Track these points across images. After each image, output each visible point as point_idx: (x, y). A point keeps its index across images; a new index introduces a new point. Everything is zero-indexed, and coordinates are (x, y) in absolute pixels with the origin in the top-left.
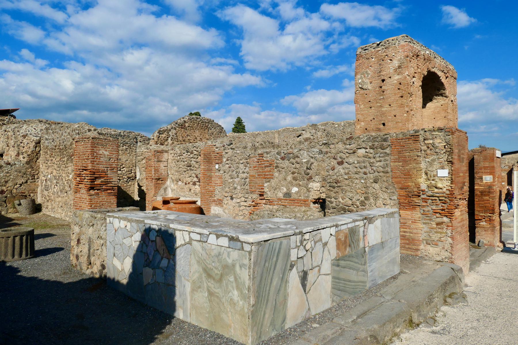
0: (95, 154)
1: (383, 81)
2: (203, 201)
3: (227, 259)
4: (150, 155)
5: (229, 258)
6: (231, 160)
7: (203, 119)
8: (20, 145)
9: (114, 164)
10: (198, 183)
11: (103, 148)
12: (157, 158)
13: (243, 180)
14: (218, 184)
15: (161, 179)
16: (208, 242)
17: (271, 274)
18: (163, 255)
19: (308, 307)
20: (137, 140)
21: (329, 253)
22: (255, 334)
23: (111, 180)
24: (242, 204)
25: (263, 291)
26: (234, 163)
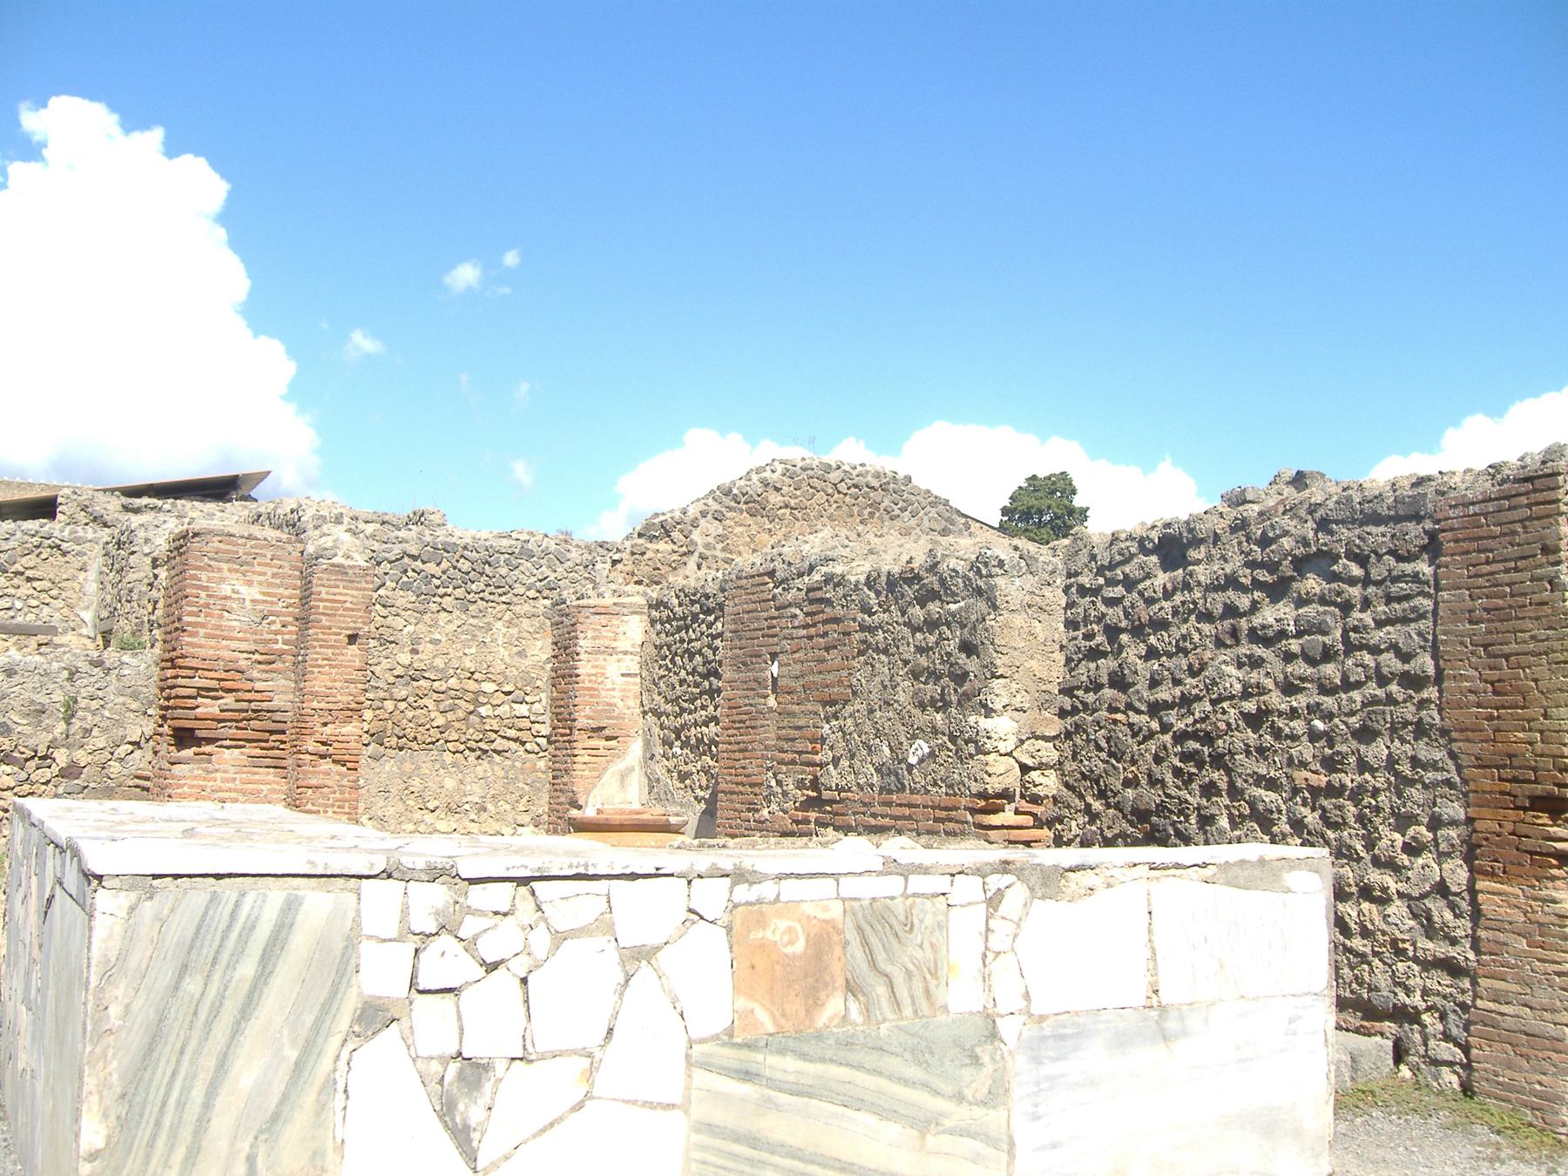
0: (203, 594)
7: (855, 473)
9: (279, 637)
11: (236, 571)
12: (594, 638)
15: (607, 732)
25: (164, 1104)
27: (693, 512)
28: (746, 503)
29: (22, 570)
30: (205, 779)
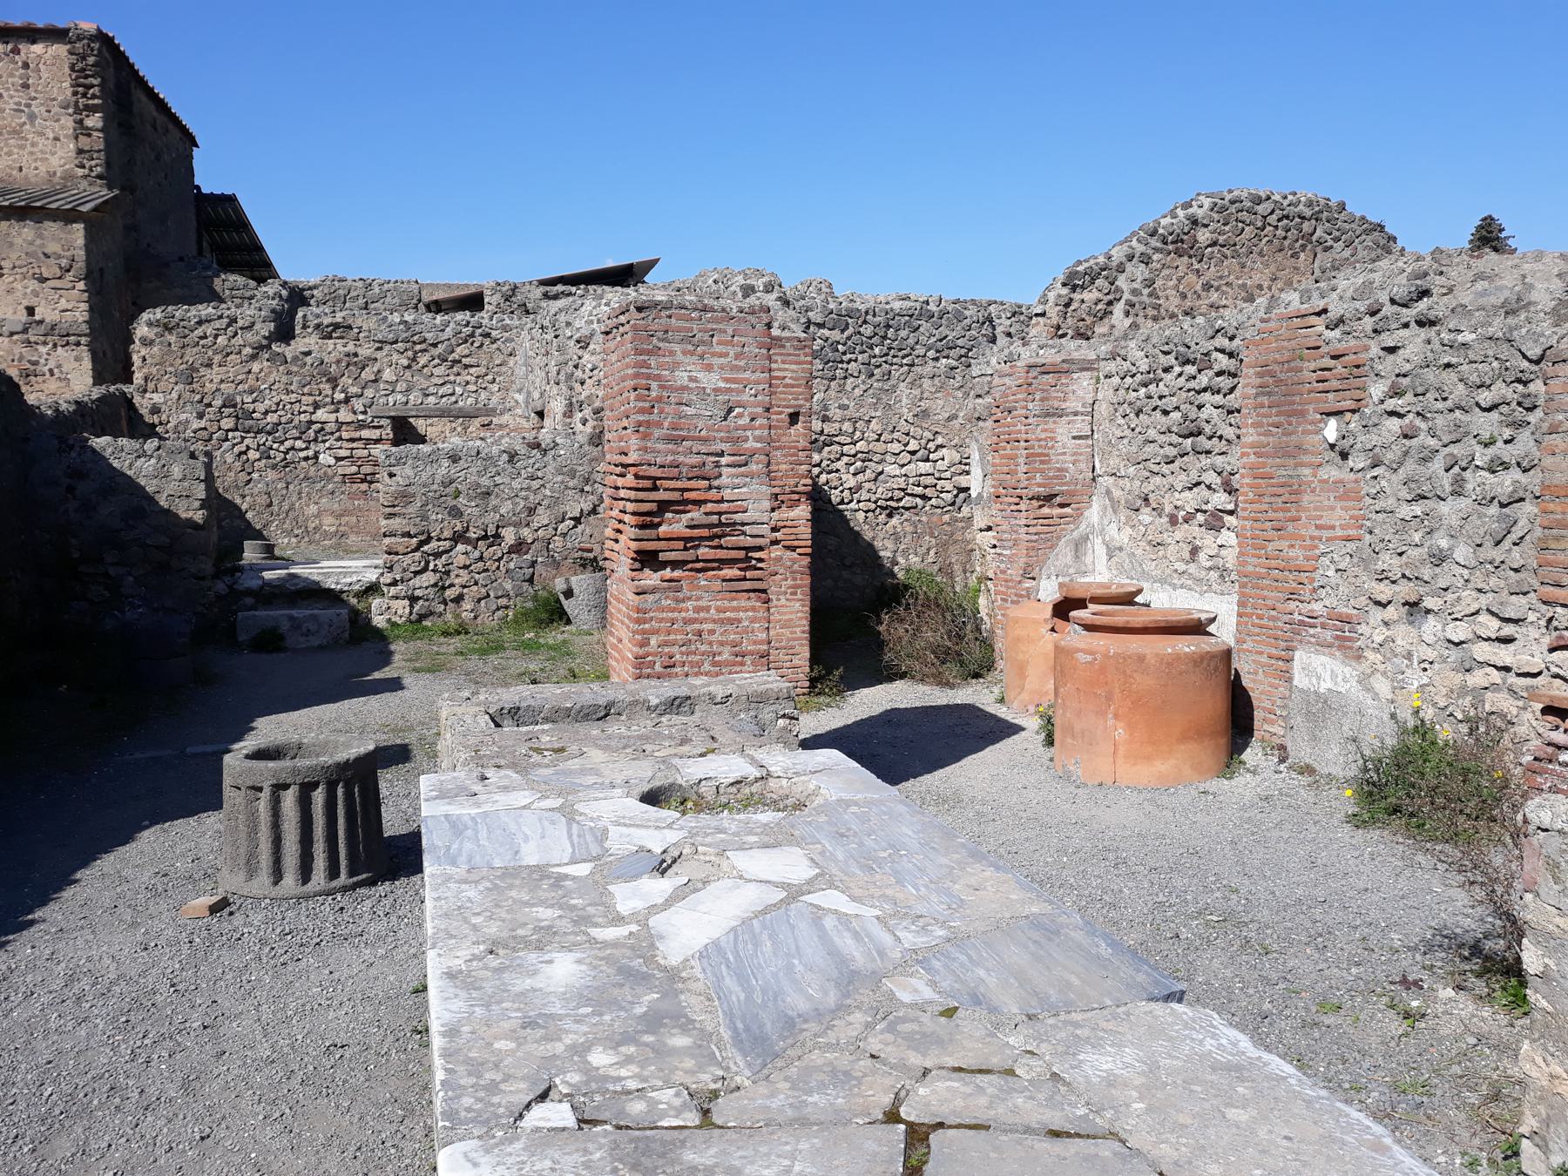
1: (949, 1013)
2: (1250, 616)
4: (1010, 388)
6: (1420, 390)
7: (1286, 203)
8: (572, 375)
9: (749, 433)
11: (692, 353)
12: (1042, 400)
13: (1494, 510)
14: (1333, 528)
15: (1058, 500)
20: (994, 328)
23: (738, 517)
24: (1482, 651)
26: (1440, 405)
27: (1118, 254)
28: (1172, 243)
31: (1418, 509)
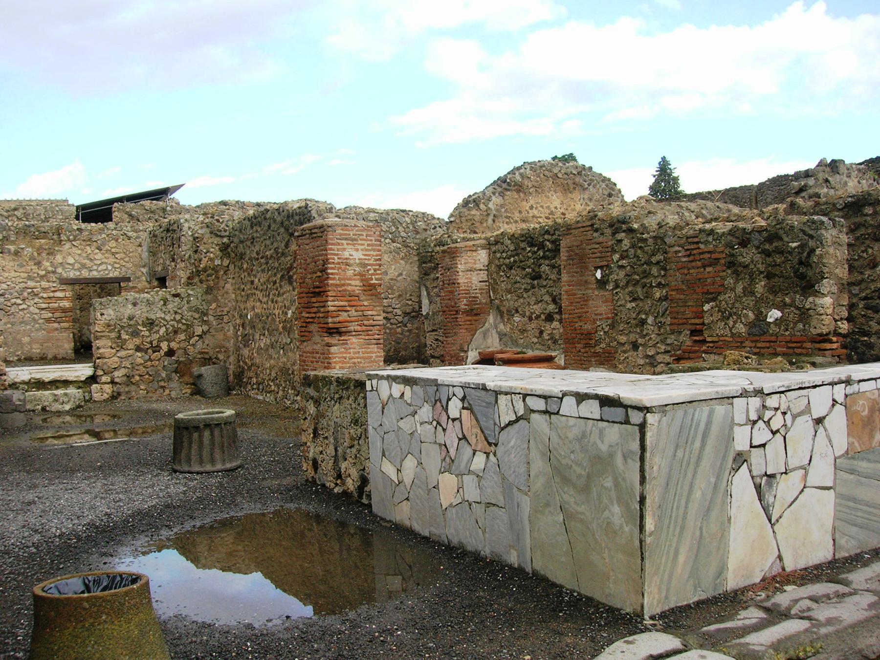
0: (336, 258)
3: (599, 443)
5: (603, 442)
9: (373, 277)
10: (557, 317)
12: (465, 263)
14: (601, 314)
16: (560, 413)
17: (690, 475)
18: (476, 445)
19: (778, 553)
21: (830, 441)
22: (656, 590)
29: (109, 248)
30: (345, 353)
31: (634, 304)
